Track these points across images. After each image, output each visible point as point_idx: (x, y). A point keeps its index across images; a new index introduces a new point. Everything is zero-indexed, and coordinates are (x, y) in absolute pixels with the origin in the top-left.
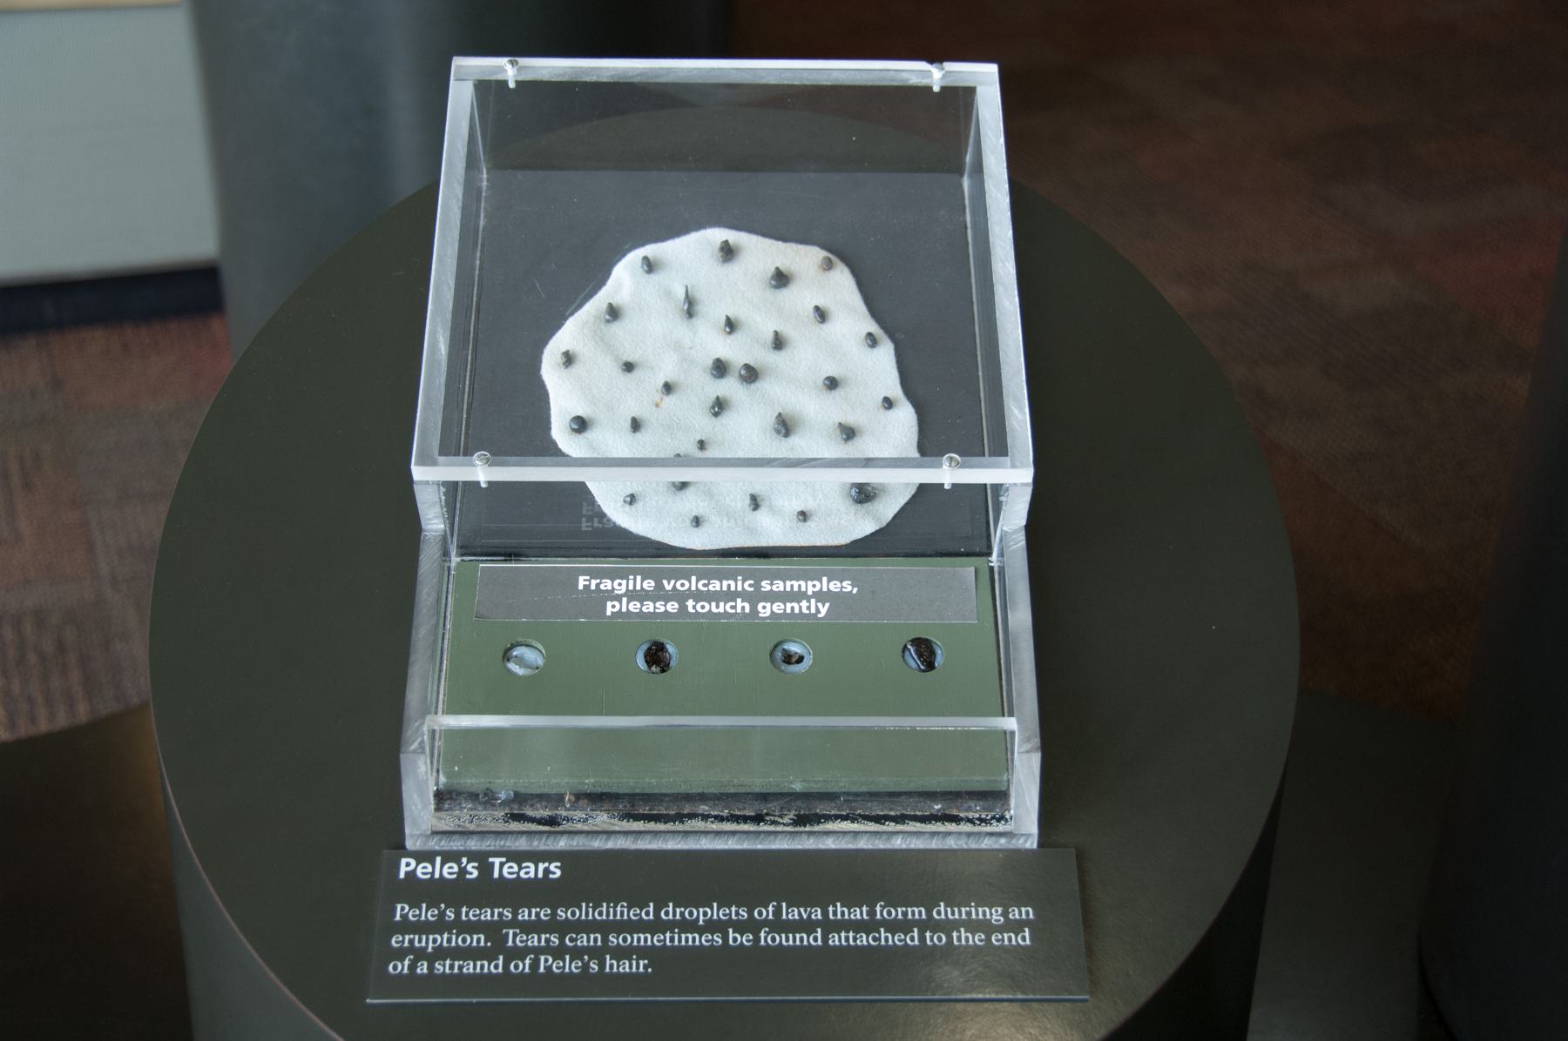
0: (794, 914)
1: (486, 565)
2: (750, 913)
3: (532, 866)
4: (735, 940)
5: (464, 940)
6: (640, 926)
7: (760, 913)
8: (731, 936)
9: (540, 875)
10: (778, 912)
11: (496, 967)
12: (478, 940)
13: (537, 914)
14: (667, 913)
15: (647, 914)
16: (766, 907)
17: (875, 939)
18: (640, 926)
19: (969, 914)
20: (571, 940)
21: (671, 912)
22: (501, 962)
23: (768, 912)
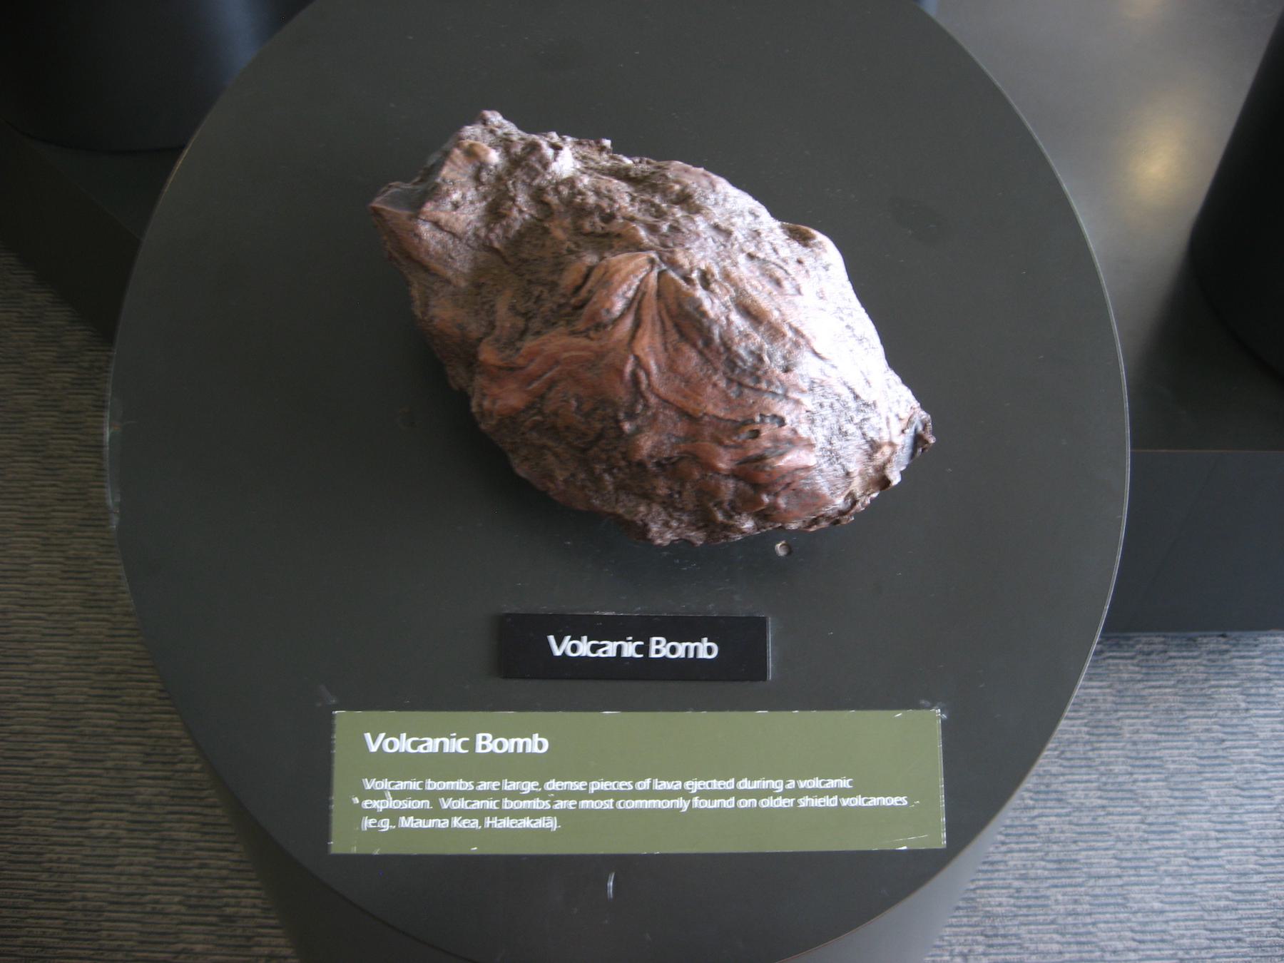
1: (637, 283)
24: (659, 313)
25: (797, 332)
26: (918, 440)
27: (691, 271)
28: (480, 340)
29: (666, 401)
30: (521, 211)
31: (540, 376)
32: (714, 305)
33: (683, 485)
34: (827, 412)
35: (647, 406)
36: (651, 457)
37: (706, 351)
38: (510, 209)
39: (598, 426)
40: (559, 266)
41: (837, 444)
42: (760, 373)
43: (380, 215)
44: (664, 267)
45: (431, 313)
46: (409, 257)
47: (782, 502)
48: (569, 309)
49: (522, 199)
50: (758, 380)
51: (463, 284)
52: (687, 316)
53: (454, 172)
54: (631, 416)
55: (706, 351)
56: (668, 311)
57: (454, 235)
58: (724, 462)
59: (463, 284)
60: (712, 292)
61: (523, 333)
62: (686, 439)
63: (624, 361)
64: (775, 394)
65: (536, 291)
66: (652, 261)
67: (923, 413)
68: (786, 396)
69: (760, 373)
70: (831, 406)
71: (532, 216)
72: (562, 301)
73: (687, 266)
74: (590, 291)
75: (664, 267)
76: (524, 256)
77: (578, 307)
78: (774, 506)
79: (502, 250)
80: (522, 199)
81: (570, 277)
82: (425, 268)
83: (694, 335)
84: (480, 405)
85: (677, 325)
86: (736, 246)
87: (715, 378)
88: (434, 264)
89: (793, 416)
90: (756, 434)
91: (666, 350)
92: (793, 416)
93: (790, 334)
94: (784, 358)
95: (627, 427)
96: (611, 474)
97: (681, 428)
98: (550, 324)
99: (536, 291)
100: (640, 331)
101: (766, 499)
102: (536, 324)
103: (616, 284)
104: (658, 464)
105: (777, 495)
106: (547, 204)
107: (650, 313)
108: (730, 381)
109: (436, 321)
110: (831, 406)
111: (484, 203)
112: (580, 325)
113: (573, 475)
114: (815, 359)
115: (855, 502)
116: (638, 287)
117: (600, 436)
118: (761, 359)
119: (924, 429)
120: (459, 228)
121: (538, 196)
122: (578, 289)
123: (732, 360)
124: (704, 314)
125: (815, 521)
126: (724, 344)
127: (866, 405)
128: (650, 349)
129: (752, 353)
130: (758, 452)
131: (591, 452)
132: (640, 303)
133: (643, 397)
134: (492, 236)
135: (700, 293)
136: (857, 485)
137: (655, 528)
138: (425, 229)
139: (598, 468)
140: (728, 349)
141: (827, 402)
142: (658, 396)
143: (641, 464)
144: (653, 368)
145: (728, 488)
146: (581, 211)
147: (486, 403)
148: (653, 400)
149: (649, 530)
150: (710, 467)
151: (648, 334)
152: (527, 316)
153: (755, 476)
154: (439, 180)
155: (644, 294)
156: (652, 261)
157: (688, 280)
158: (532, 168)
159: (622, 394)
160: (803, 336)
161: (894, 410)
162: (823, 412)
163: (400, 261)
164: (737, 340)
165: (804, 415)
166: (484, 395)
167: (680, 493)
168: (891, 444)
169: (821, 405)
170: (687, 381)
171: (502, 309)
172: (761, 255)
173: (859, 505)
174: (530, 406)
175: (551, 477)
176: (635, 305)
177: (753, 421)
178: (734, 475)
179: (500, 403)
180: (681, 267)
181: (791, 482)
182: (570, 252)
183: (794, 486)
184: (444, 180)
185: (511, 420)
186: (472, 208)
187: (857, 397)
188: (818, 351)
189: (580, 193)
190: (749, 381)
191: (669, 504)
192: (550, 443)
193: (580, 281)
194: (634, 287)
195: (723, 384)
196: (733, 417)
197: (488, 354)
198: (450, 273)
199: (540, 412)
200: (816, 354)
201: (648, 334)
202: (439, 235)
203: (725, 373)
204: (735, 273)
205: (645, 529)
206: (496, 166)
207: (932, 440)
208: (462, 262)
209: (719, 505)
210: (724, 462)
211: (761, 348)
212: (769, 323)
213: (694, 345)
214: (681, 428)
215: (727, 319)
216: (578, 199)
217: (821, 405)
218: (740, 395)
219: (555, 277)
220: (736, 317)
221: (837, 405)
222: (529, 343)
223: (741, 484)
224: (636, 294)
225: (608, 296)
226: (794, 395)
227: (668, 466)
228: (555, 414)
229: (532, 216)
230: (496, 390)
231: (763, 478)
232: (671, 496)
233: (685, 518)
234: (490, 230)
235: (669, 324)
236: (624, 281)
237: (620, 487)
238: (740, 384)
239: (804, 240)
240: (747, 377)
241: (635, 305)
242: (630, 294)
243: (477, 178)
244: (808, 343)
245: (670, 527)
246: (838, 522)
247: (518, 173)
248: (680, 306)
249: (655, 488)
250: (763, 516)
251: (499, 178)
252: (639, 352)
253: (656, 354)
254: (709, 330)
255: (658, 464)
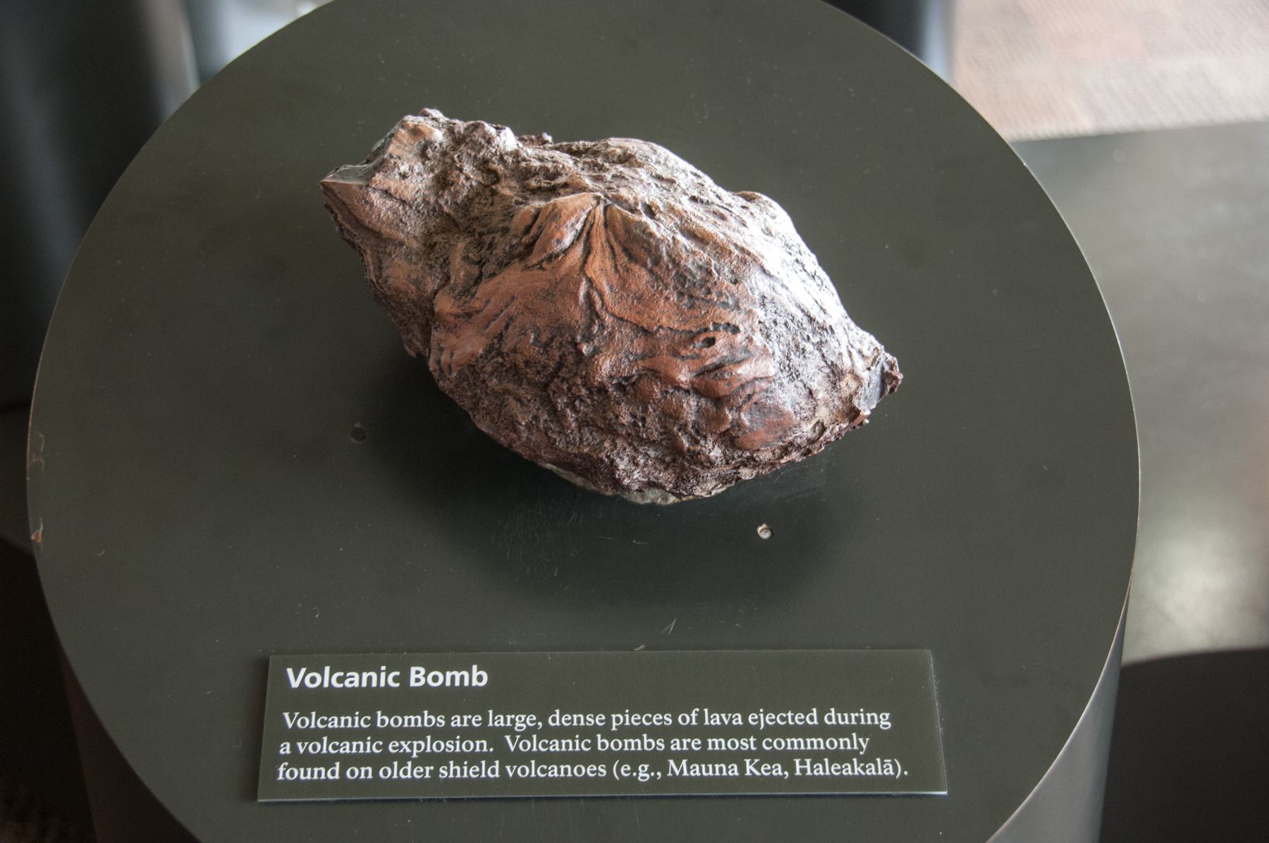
0: (715, 720)
1: (585, 216)
2: (675, 719)
3: (356, 675)
4: (603, 745)
5: (468, 746)
6: (805, 731)
7: (684, 719)
8: (599, 741)
9: (364, 684)
10: (700, 718)
11: (333, 773)
12: (481, 745)
13: (469, 721)
14: (830, 719)
15: (812, 719)
16: (689, 713)
17: (782, 719)
18: (805, 731)
19: (858, 719)
20: (768, 744)
21: (833, 717)
22: (337, 769)
23: (691, 718)
24: (608, 241)
25: (742, 250)
26: (885, 377)
27: (637, 204)
28: (436, 292)
29: (621, 319)
30: (467, 178)
31: (497, 315)
32: (661, 229)
33: (645, 410)
34: (781, 329)
35: (602, 327)
36: (611, 377)
37: (656, 269)
38: (458, 176)
39: (557, 354)
40: (509, 215)
41: (796, 360)
42: (709, 285)
43: (331, 190)
44: (609, 202)
45: (384, 275)
46: (359, 224)
47: (745, 418)
48: (521, 249)
49: (468, 168)
50: (709, 292)
51: (415, 245)
52: (636, 239)
53: (401, 152)
54: (588, 338)
55: (656, 269)
56: (616, 238)
57: (403, 202)
58: (684, 376)
59: (415, 245)
60: (659, 220)
61: (478, 280)
62: (643, 357)
63: (578, 283)
64: (725, 305)
65: (487, 239)
66: (598, 198)
67: (888, 355)
68: (737, 307)
69: (709, 285)
70: (786, 324)
71: (479, 183)
72: (514, 242)
73: (632, 201)
74: (540, 227)
75: (609, 202)
76: (473, 215)
77: (530, 243)
78: (738, 424)
79: (452, 213)
80: (468, 168)
81: (518, 222)
82: (377, 235)
83: (642, 254)
84: (439, 362)
85: (625, 250)
86: (679, 190)
87: (666, 293)
88: (386, 230)
89: (746, 325)
90: (711, 342)
91: (617, 271)
92: (746, 325)
93: (736, 252)
94: (732, 272)
95: (585, 349)
96: (574, 409)
97: (638, 346)
98: (503, 265)
99: (487, 239)
100: (591, 257)
101: (730, 416)
102: (489, 268)
103: (564, 217)
104: (620, 387)
105: (739, 409)
106: (494, 172)
107: (599, 242)
108: (681, 294)
109: (391, 281)
110: (786, 324)
111: (431, 175)
112: (534, 260)
113: (536, 418)
114: (763, 276)
115: (824, 429)
116: (586, 219)
117: (560, 365)
118: (710, 273)
119: (892, 368)
120: (408, 195)
121: (483, 166)
122: (528, 230)
123: (682, 277)
124: (651, 235)
125: (785, 451)
126: (673, 261)
127: (823, 328)
128: (599, 266)
129: (700, 267)
130: (715, 360)
131: (552, 386)
132: (589, 233)
133: (598, 316)
134: (442, 202)
135: (645, 218)
136: (823, 414)
137: (622, 465)
138: (375, 197)
139: (561, 402)
140: (676, 264)
141: (781, 320)
142: (613, 315)
143: (602, 390)
144: (607, 289)
145: (690, 407)
146: (529, 173)
147: (445, 358)
148: (608, 320)
149: (617, 468)
150: (670, 382)
151: (598, 258)
152: (481, 263)
153: (713, 388)
154: (386, 156)
155: (592, 226)
156: (598, 198)
157: (633, 210)
158: (475, 143)
159: (577, 316)
160: (749, 254)
161: (860, 350)
162: (778, 329)
163: (351, 230)
164: (684, 256)
165: (757, 326)
166: (441, 350)
167: (644, 419)
168: (857, 378)
169: (775, 322)
170: (640, 299)
171: (457, 260)
172: (705, 198)
173: (827, 433)
174: (489, 349)
175: (513, 425)
176: (585, 236)
177: (706, 330)
178: (696, 390)
179: (457, 353)
180: (626, 201)
181: (748, 395)
182: (517, 203)
183: (755, 398)
184: (391, 157)
185: (472, 369)
186: (420, 178)
187: (811, 320)
188: (766, 267)
189: (524, 160)
190: (700, 293)
191: (636, 439)
192: (511, 387)
193: (529, 222)
194: (582, 219)
195: (674, 298)
196: (687, 328)
197: (445, 305)
198: (402, 236)
199: (500, 354)
200: (764, 271)
201: (598, 258)
202: (389, 203)
203: (675, 288)
204: (678, 207)
205: (612, 466)
206: (441, 144)
207: (900, 377)
208: (413, 227)
209: (683, 428)
210: (684, 376)
211: (709, 263)
212: (715, 243)
213: (645, 265)
214: (638, 346)
215: (674, 238)
216: (523, 164)
217: (775, 322)
218: (692, 307)
219: (506, 223)
220: (679, 237)
221: (791, 324)
222: (486, 287)
223: (703, 401)
224: (584, 226)
225: (558, 228)
226: (744, 305)
227: (629, 387)
228: (515, 351)
229: (479, 183)
230: (453, 340)
231: (723, 389)
232: (635, 424)
233: (652, 453)
234: (438, 196)
235: (618, 249)
236: (569, 217)
237: (583, 423)
238: (691, 297)
239: (750, 199)
240: (695, 289)
241: (584, 234)
242: (579, 226)
243: (423, 155)
244: (755, 260)
245: (637, 465)
246: (809, 451)
247: (462, 147)
248: (628, 231)
249: (617, 417)
250: (730, 440)
251: (444, 154)
252: (590, 274)
253: (606, 275)
254: (657, 248)
255: (620, 387)
